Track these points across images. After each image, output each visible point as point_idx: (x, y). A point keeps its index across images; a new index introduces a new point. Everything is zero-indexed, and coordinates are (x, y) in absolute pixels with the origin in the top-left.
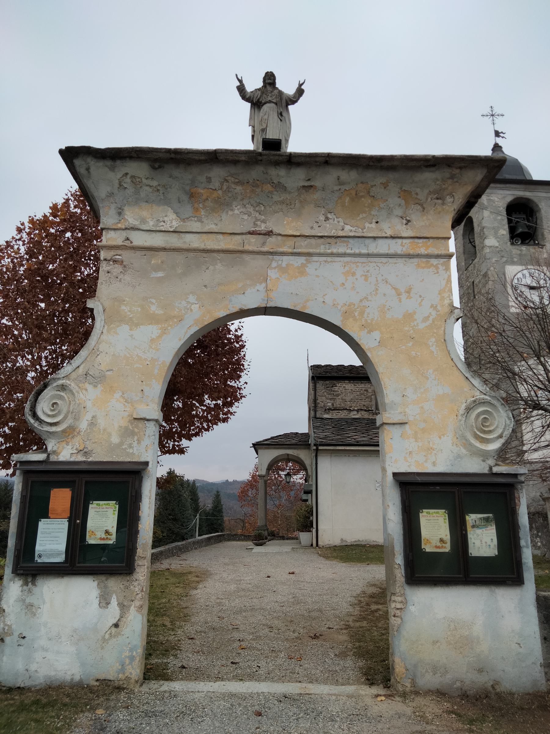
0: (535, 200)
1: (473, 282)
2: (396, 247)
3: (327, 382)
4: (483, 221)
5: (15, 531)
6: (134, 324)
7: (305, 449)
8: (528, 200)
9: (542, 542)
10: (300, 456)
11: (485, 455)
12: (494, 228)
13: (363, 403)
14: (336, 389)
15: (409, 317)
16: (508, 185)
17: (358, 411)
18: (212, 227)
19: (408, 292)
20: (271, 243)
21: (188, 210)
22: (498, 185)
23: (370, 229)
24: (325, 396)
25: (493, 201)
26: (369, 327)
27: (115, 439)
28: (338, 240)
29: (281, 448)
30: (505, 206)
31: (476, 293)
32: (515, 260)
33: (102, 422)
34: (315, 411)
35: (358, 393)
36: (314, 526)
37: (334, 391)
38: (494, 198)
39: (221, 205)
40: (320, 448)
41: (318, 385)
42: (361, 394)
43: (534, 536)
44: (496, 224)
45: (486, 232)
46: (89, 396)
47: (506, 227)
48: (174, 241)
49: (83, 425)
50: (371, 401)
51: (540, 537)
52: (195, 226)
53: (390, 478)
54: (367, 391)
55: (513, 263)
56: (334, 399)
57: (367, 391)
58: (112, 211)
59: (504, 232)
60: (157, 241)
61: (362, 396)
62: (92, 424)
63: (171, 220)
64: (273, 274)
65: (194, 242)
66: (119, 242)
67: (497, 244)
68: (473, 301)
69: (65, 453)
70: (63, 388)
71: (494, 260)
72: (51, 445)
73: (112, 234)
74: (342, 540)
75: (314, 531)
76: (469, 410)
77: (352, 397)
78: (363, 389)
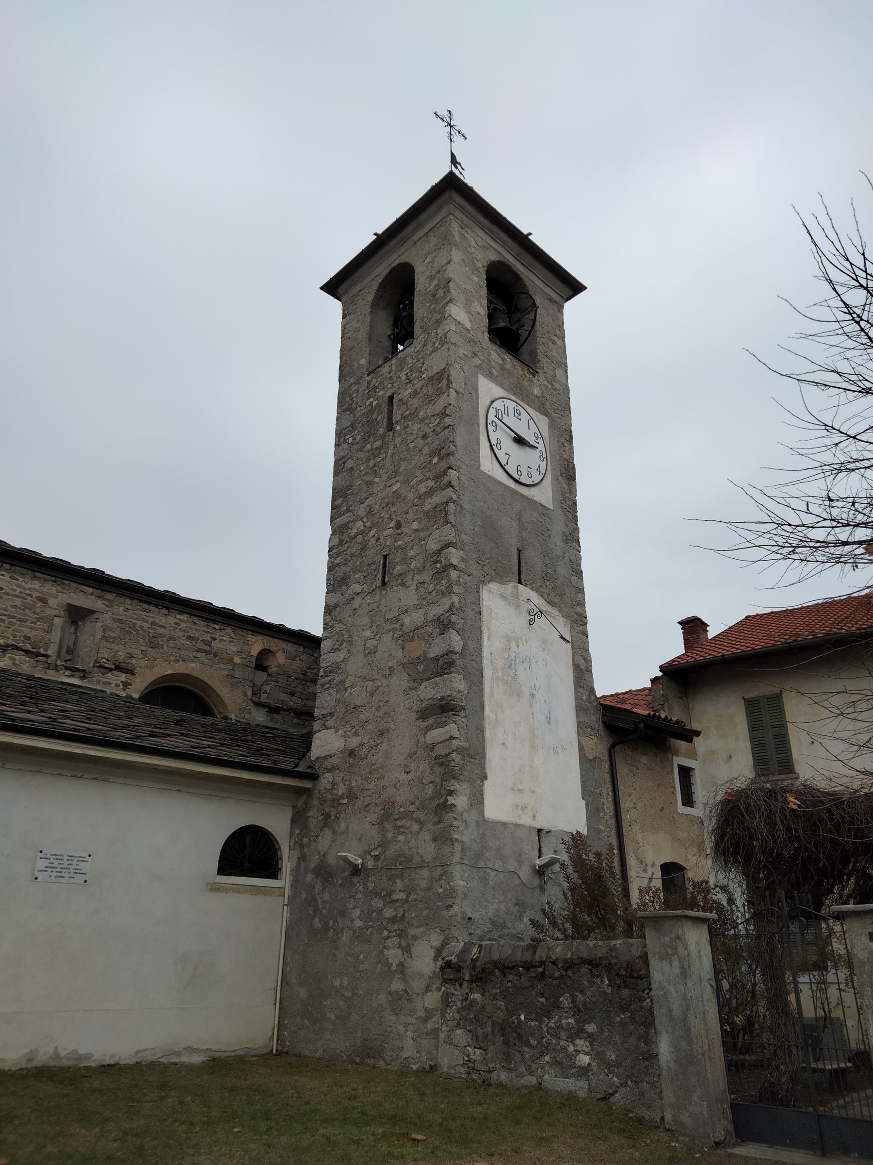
1: (391, 398)
4: (450, 268)
5: (247, 772)
9: (599, 1056)
13: (26, 632)
16: (495, 229)
22: (481, 219)
31: (396, 417)
42: (26, 606)
43: (563, 1035)
50: (49, 631)
51: (591, 1038)
53: (287, 864)
54: (44, 601)
57: (44, 601)
61: (28, 612)
67: (468, 325)
68: (383, 437)
71: (461, 351)
78: (35, 594)
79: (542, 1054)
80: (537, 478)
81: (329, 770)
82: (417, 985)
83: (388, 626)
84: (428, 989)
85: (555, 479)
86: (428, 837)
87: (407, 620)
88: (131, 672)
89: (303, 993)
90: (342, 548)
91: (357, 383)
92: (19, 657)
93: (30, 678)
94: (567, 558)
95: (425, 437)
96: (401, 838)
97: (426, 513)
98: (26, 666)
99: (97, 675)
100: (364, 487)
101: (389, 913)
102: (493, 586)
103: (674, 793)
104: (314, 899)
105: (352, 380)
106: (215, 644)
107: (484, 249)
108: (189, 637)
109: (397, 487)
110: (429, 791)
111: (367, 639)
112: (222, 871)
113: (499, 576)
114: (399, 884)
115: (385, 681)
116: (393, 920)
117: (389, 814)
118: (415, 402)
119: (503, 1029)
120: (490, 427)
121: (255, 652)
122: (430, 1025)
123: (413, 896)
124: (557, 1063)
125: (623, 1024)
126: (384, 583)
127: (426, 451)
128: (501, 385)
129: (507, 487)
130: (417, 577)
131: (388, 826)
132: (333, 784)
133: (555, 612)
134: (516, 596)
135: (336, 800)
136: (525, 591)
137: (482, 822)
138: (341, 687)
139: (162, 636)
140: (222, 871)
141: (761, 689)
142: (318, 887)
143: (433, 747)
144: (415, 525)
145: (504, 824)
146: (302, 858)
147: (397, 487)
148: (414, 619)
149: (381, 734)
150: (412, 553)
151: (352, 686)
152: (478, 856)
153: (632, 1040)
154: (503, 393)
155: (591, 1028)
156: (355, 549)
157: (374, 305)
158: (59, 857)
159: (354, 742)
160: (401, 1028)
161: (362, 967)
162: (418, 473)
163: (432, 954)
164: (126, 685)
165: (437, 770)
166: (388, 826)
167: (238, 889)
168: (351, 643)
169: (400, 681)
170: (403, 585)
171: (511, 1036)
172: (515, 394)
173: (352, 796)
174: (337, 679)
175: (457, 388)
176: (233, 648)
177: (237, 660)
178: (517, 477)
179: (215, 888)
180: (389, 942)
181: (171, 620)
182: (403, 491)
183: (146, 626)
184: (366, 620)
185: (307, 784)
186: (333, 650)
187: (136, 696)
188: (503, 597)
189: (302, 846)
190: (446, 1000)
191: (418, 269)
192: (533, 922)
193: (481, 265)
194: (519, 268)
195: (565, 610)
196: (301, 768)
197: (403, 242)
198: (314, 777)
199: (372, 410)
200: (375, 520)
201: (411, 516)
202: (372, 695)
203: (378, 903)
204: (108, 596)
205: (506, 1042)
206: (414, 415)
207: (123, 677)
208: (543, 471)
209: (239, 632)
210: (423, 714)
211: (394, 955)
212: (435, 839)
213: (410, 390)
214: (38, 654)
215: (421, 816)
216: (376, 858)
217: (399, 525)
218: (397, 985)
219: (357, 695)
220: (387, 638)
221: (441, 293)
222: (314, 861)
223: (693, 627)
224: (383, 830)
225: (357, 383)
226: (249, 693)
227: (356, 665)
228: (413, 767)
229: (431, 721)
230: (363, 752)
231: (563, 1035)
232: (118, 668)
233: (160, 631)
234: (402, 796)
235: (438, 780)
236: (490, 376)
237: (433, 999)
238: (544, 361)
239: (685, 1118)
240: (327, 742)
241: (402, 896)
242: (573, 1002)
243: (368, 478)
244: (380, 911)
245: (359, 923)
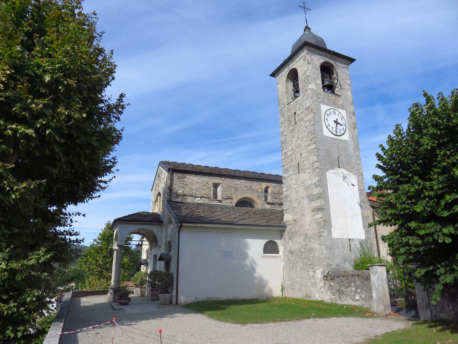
1: (295, 113)
7: (157, 225)
8: (331, 65)
9: (361, 297)
10: (153, 231)
13: (205, 192)
14: (186, 180)
16: (322, 52)
17: (201, 197)
22: (317, 51)
24: (178, 185)
30: (320, 65)
31: (297, 120)
32: (326, 101)
34: (170, 196)
35: (202, 185)
36: (175, 287)
37: (184, 181)
40: (184, 225)
42: (204, 185)
43: (352, 292)
47: (320, 79)
50: (210, 191)
54: (208, 183)
56: (184, 188)
57: (208, 183)
67: (316, 89)
74: (196, 298)
75: (174, 291)
77: (197, 186)
79: (348, 296)
80: (343, 132)
81: (289, 225)
82: (318, 281)
83: (301, 185)
84: (320, 282)
86: (317, 243)
87: (306, 183)
88: (232, 199)
89: (289, 283)
90: (286, 160)
91: (284, 107)
92: (205, 199)
93: (208, 205)
94: (355, 156)
95: (306, 127)
96: (310, 243)
97: (309, 151)
98: (206, 201)
99: (224, 201)
100: (290, 141)
101: (309, 263)
102: (331, 171)
104: (289, 259)
105: (283, 106)
106: (253, 187)
107: (318, 60)
108: (246, 186)
109: (299, 142)
110: (317, 232)
111: (296, 188)
112: (264, 253)
113: (332, 167)
114: (311, 256)
115: (302, 201)
116: (310, 265)
117: (306, 236)
118: (302, 116)
119: (339, 291)
120: (326, 121)
122: (322, 290)
123: (315, 259)
124: (351, 298)
125: (365, 290)
126: (299, 172)
127: (307, 131)
128: (328, 105)
129: (332, 138)
130: (308, 171)
131: (307, 240)
132: (291, 229)
133: (351, 174)
134: (338, 173)
135: (292, 233)
136: (341, 170)
137: (332, 239)
138: (290, 202)
139: (238, 187)
140: (264, 253)
142: (290, 256)
143: (316, 220)
144: (306, 155)
145: (339, 239)
146: (285, 248)
147: (299, 142)
148: (308, 183)
149: (302, 215)
150: (306, 163)
151: (293, 201)
152: (331, 248)
153: (368, 293)
154: (330, 107)
155: (359, 291)
156: (290, 160)
157: (287, 81)
158: (226, 252)
159: (295, 217)
160: (315, 291)
161: (304, 276)
162: (305, 138)
163: (321, 273)
164: (231, 202)
165: (318, 225)
166: (307, 240)
167: (269, 257)
168: (291, 188)
169: (306, 201)
170: (304, 173)
171: (340, 292)
172: (333, 106)
173: (296, 232)
174: (289, 199)
175: (314, 111)
176: (258, 187)
177: (259, 191)
178: (336, 134)
179: (263, 257)
180: (310, 270)
182: (301, 144)
183: (234, 185)
184: (295, 182)
185: (284, 229)
186: (287, 191)
187: (234, 205)
188: (334, 173)
189: (284, 245)
190: (325, 284)
191: (299, 71)
193: (318, 66)
194: (331, 62)
195: (355, 172)
196: (281, 225)
197: (293, 61)
198: (286, 227)
199: (290, 117)
200: (294, 152)
201: (304, 152)
202: (299, 204)
203: (306, 260)
205: (340, 294)
206: (302, 119)
207: (230, 201)
208: (345, 129)
210: (313, 211)
211: (311, 273)
212: (319, 244)
213: (300, 112)
214: (209, 198)
215: (315, 238)
216: (304, 249)
217: (301, 154)
218: (313, 281)
219: (295, 204)
220: (301, 188)
221: (306, 80)
222: (288, 249)
224: (305, 241)
225: (284, 107)
226: (264, 200)
227: (293, 195)
228: (312, 225)
229: (315, 212)
230: (298, 220)
231: (352, 292)
232: (228, 198)
233: (238, 186)
234: (310, 232)
235: (318, 229)
236: (324, 103)
237: (322, 284)
239: (379, 310)
240: (287, 217)
241: (312, 259)
242: (354, 285)
243: (291, 138)
244: (307, 262)
245: (301, 265)
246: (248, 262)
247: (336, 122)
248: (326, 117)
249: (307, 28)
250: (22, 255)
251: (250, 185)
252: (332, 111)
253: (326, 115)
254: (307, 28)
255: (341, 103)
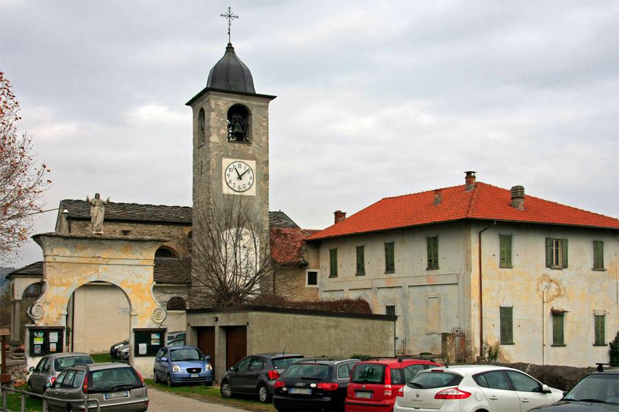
0: (249, 107)
2: (138, 262)
3: (81, 222)
6: (58, 286)
11: (158, 323)
12: (217, 128)
15: (140, 284)
18: (81, 255)
19: (140, 276)
20: (100, 261)
21: (74, 250)
23: (130, 256)
25: (219, 106)
26: (128, 287)
27: (55, 320)
28: (115, 243)
29: (36, 277)
32: (230, 154)
33: (50, 316)
38: (220, 103)
39: (84, 248)
41: (72, 225)
44: (219, 125)
45: (211, 131)
46: (46, 308)
48: (70, 260)
49: (45, 316)
52: (75, 255)
53: (315, 271)
55: (228, 157)
57: (115, 231)
58: (49, 250)
59: (224, 131)
60: (64, 260)
62: (48, 316)
63: (68, 253)
64: (100, 270)
65: (76, 260)
66: (52, 260)
69: (41, 324)
70: (39, 306)
72: (36, 322)
73: (49, 257)
76: (155, 311)
80: (248, 187)
85: (258, 183)
103: (305, 282)
106: (172, 233)
121: (187, 233)
141: (389, 240)
158: (124, 309)
177: (180, 237)
181: (156, 228)
192: (23, 351)
204: (134, 225)
208: (251, 183)
209: (181, 227)
223: (339, 215)
233: (152, 233)
238: (255, 137)
246: (469, 347)
247: (240, 177)
248: (228, 172)
249: (230, 48)
250: (362, 305)
251: (169, 231)
252: (236, 164)
253: (228, 170)
254: (230, 48)
255: (250, 152)
